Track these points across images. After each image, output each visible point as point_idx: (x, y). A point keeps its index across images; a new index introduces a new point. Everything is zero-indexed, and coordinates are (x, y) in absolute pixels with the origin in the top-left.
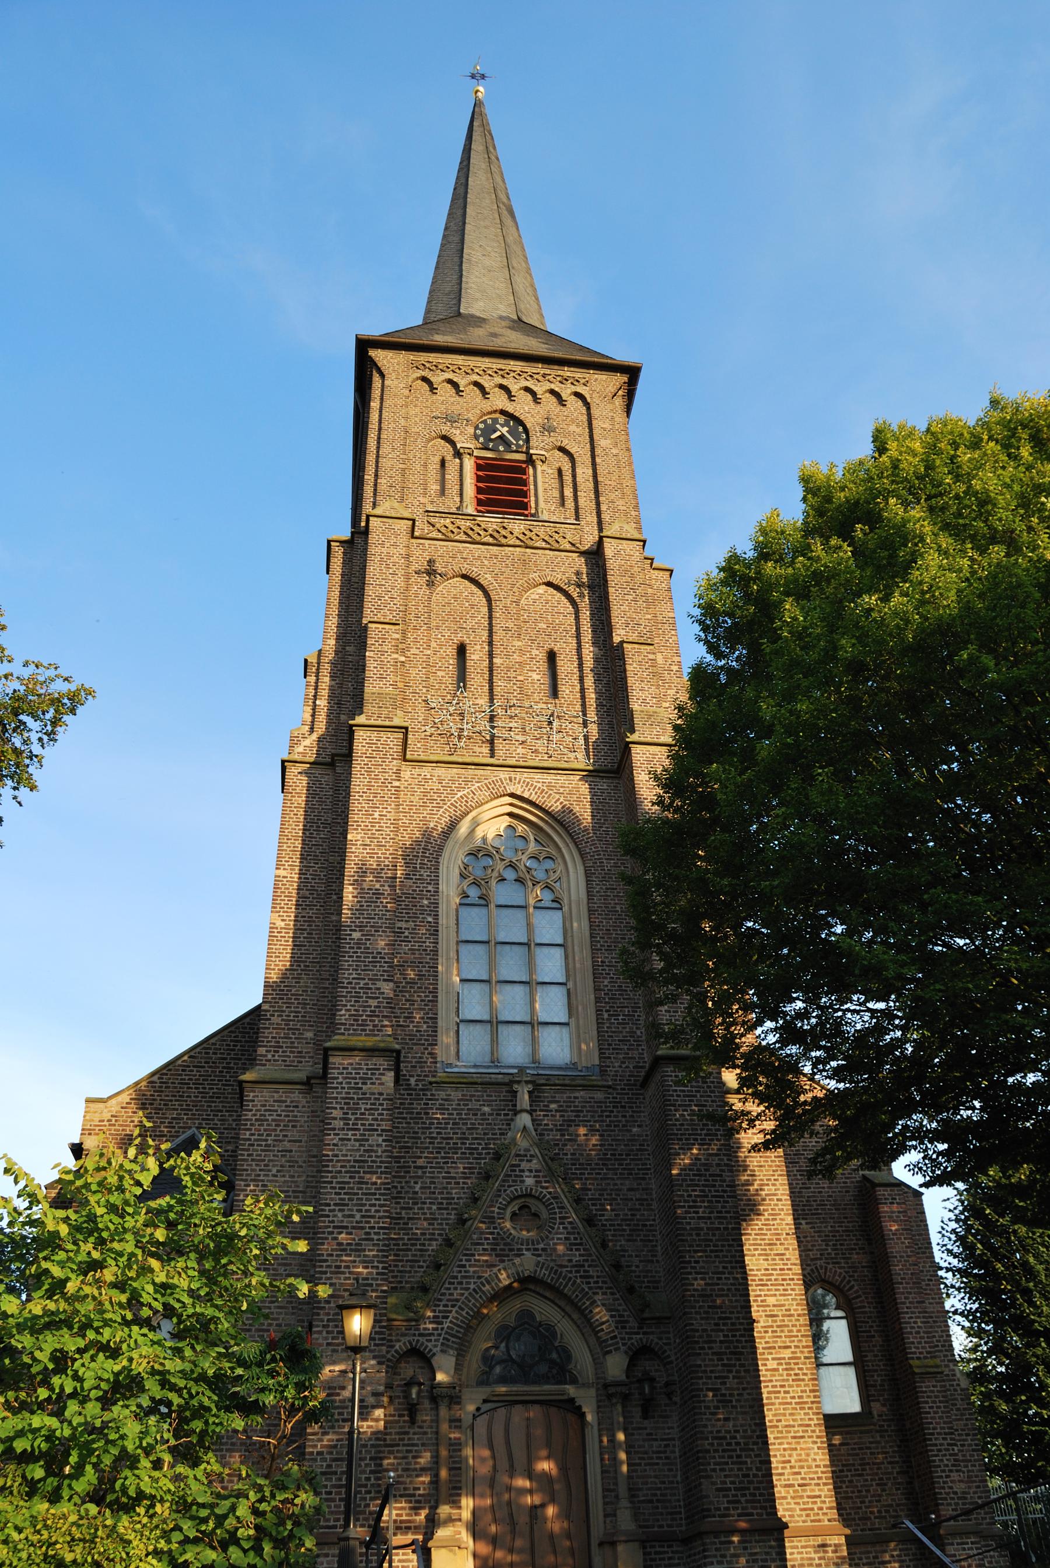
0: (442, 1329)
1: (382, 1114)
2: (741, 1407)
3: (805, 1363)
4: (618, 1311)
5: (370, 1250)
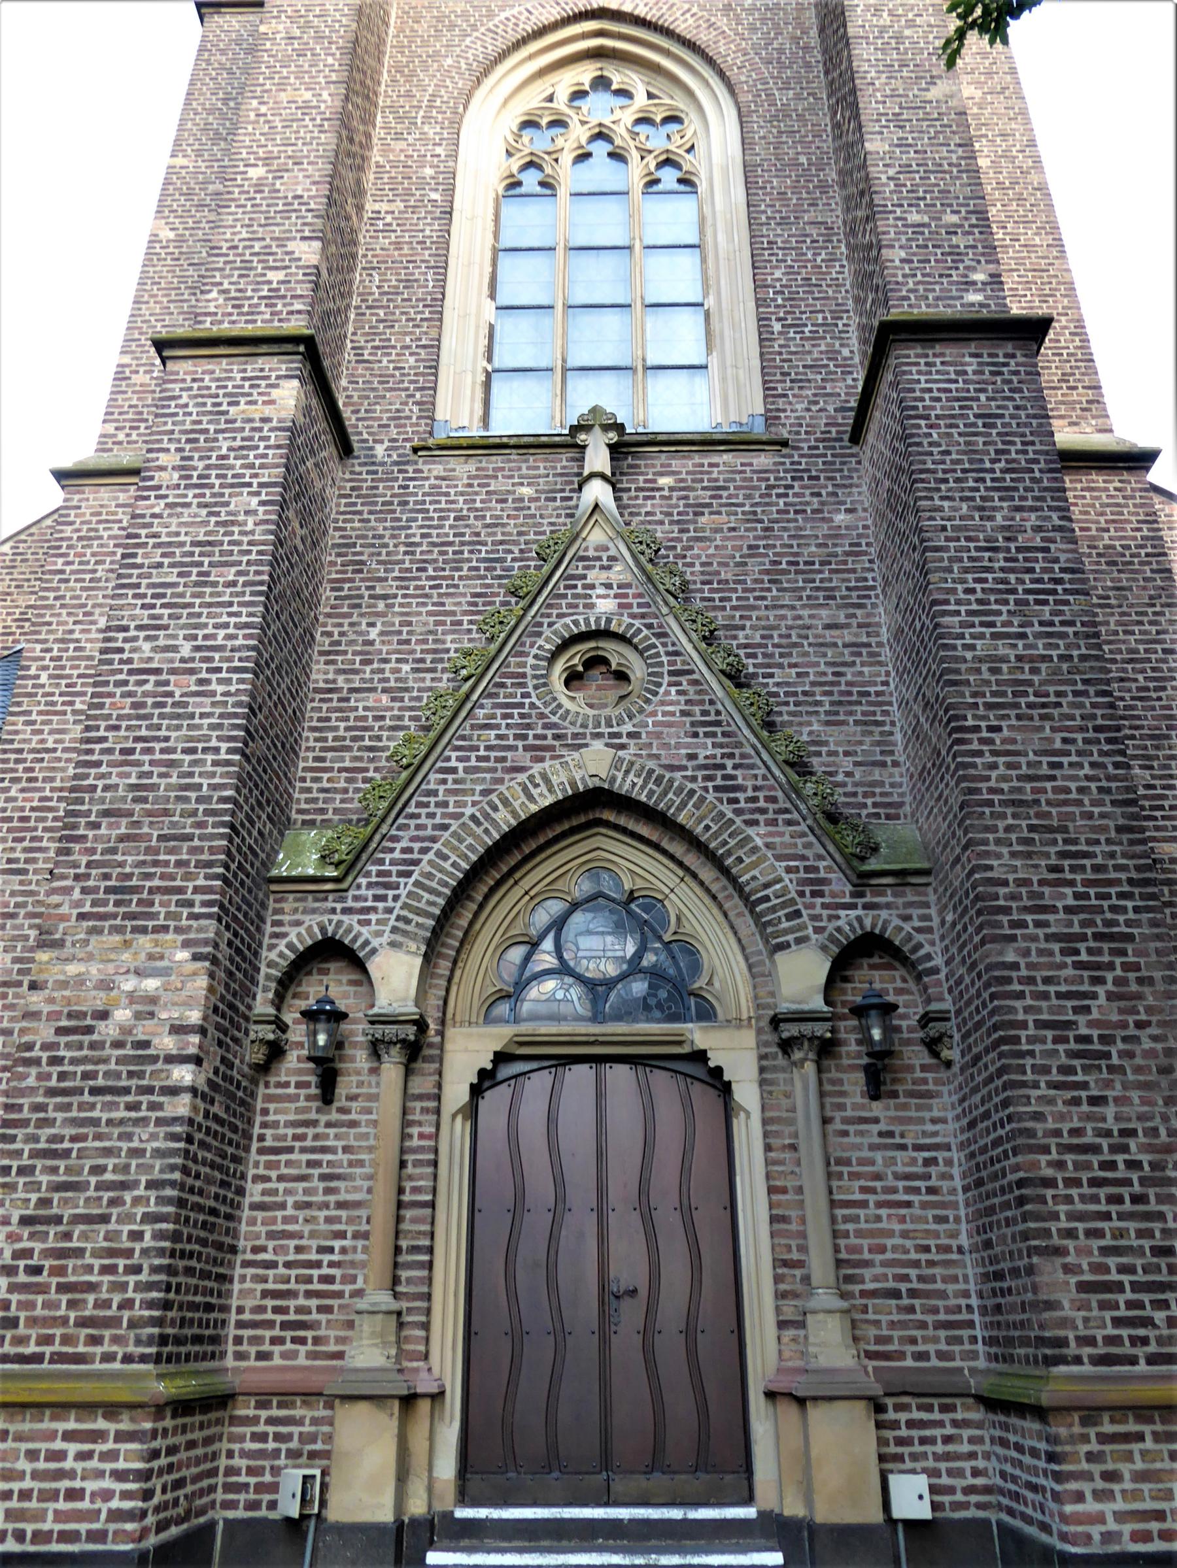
1: (265, 456)
2: (1138, 1070)
4: (803, 858)
5: (202, 716)
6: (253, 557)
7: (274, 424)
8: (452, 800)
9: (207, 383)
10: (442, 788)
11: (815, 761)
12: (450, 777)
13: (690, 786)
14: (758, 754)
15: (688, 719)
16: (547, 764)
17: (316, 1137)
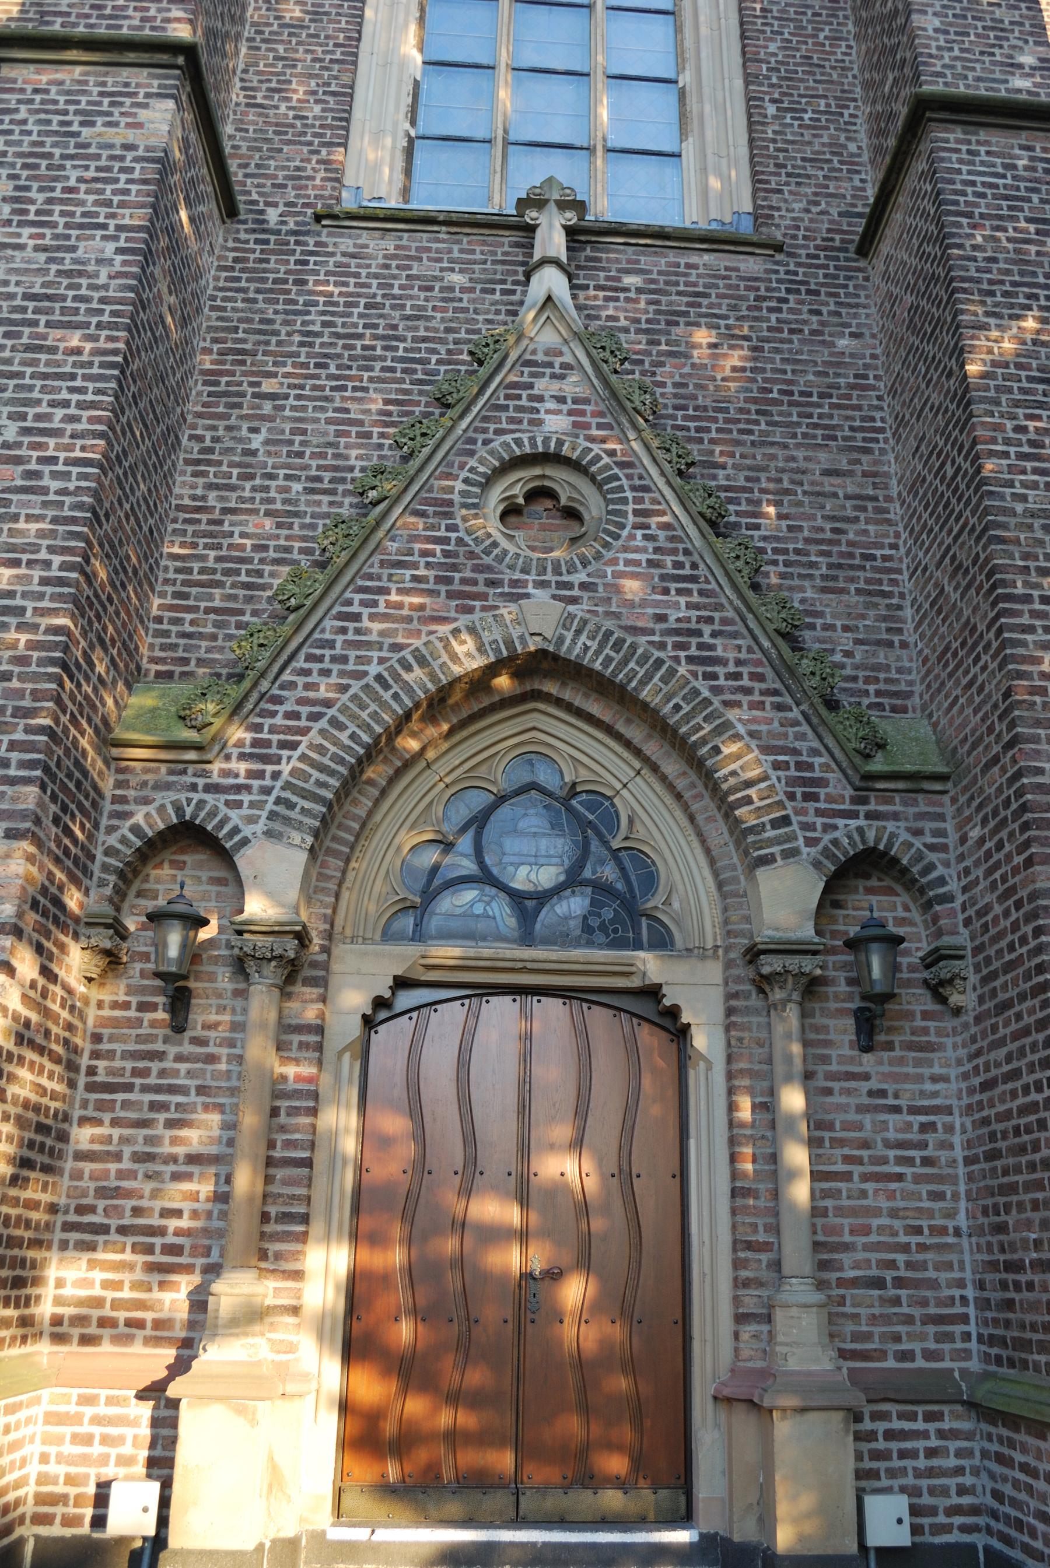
0: (276, 775)
1: (127, 192)
4: (795, 752)
5: (29, 518)
6: (106, 318)
7: (140, 153)
8: (352, 654)
9: (53, 95)
10: (340, 639)
11: (807, 634)
12: (351, 625)
13: (657, 654)
14: (744, 620)
15: (656, 572)
16: (476, 616)
17: (162, 1073)
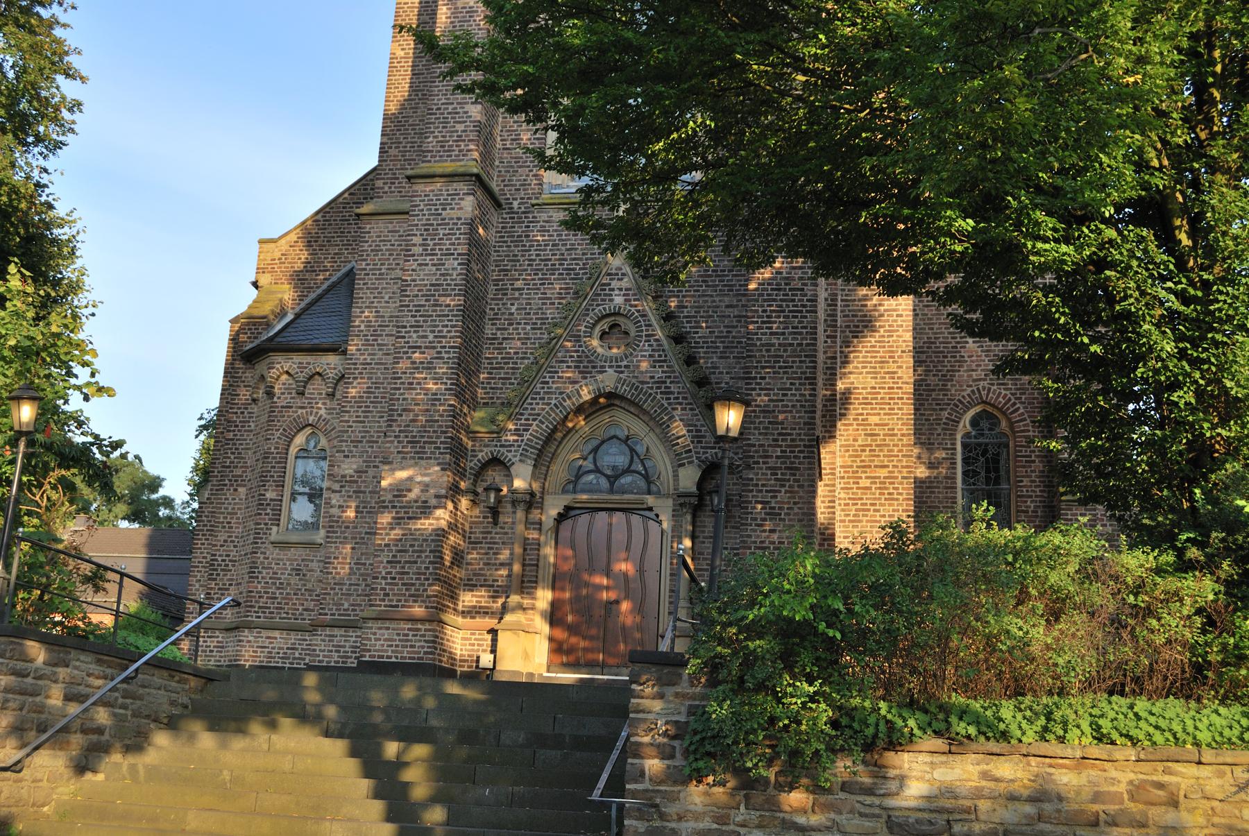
3: (902, 483)
